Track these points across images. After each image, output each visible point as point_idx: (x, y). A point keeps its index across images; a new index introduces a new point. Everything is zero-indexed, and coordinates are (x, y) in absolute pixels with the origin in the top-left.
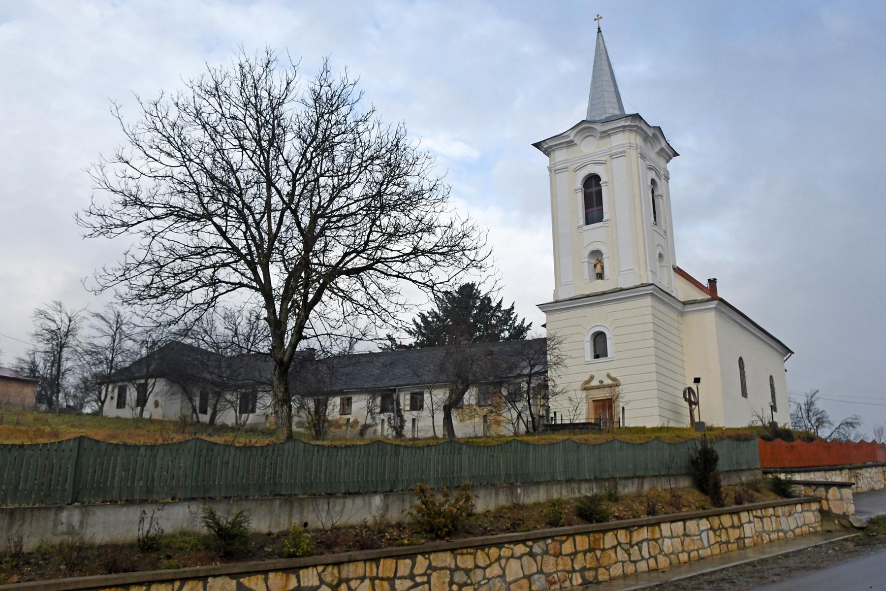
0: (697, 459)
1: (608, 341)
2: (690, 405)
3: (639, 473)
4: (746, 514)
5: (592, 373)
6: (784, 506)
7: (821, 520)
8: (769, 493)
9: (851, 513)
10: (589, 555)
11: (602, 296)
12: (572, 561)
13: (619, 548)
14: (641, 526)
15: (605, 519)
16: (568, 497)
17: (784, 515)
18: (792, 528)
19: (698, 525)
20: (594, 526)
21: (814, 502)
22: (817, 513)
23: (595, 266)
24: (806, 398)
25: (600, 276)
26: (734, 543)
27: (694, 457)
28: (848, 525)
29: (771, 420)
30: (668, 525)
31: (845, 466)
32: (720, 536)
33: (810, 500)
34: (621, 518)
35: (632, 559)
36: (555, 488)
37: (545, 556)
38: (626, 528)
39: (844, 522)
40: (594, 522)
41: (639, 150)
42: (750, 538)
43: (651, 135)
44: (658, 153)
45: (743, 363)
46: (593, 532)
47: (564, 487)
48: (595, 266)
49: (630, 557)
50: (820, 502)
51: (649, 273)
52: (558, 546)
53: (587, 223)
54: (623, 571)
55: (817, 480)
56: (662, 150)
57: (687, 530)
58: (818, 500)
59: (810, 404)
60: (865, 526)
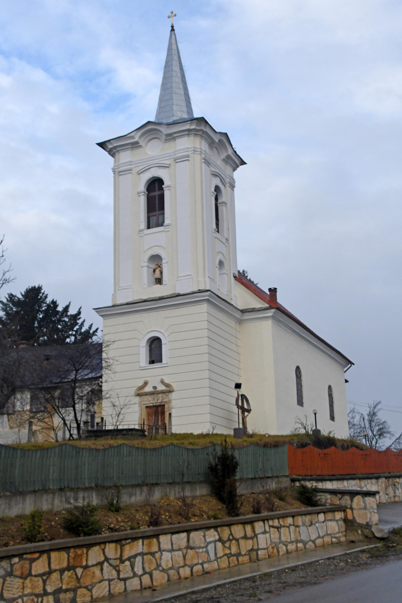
0: (217, 465)
1: (164, 347)
2: (243, 413)
3: (147, 481)
4: (261, 523)
5: (147, 379)
6: (305, 515)
7: (346, 531)
8: (293, 502)
9: (374, 523)
10: (67, 574)
11: (159, 301)
12: (44, 582)
13: (106, 564)
14: (135, 539)
15: (97, 531)
16: (61, 508)
17: (304, 524)
18: (312, 539)
19: (204, 536)
20: (82, 539)
21: (338, 511)
22: (341, 523)
23: (154, 271)
24: (368, 409)
25: (159, 281)
26: (245, 555)
27: (213, 463)
28: (370, 536)
29: (314, 428)
30: (169, 536)
31: (382, 475)
32: (230, 548)
33: (334, 509)
34: (116, 530)
35: (121, 576)
36: (45, 497)
37: (8, 578)
38: (116, 541)
39: (366, 532)
40: (82, 535)
41: (203, 155)
42: (264, 549)
43: (217, 141)
44: (224, 160)
45: (300, 372)
46: (74, 547)
47: (56, 496)
48: (154, 271)
49: (119, 575)
50: (344, 511)
51: (207, 280)
52: (27, 566)
53: (149, 227)
54: (110, 590)
55: (350, 488)
56: (228, 157)
57: (191, 541)
58: (343, 509)
59: (372, 415)
60: (386, 536)
